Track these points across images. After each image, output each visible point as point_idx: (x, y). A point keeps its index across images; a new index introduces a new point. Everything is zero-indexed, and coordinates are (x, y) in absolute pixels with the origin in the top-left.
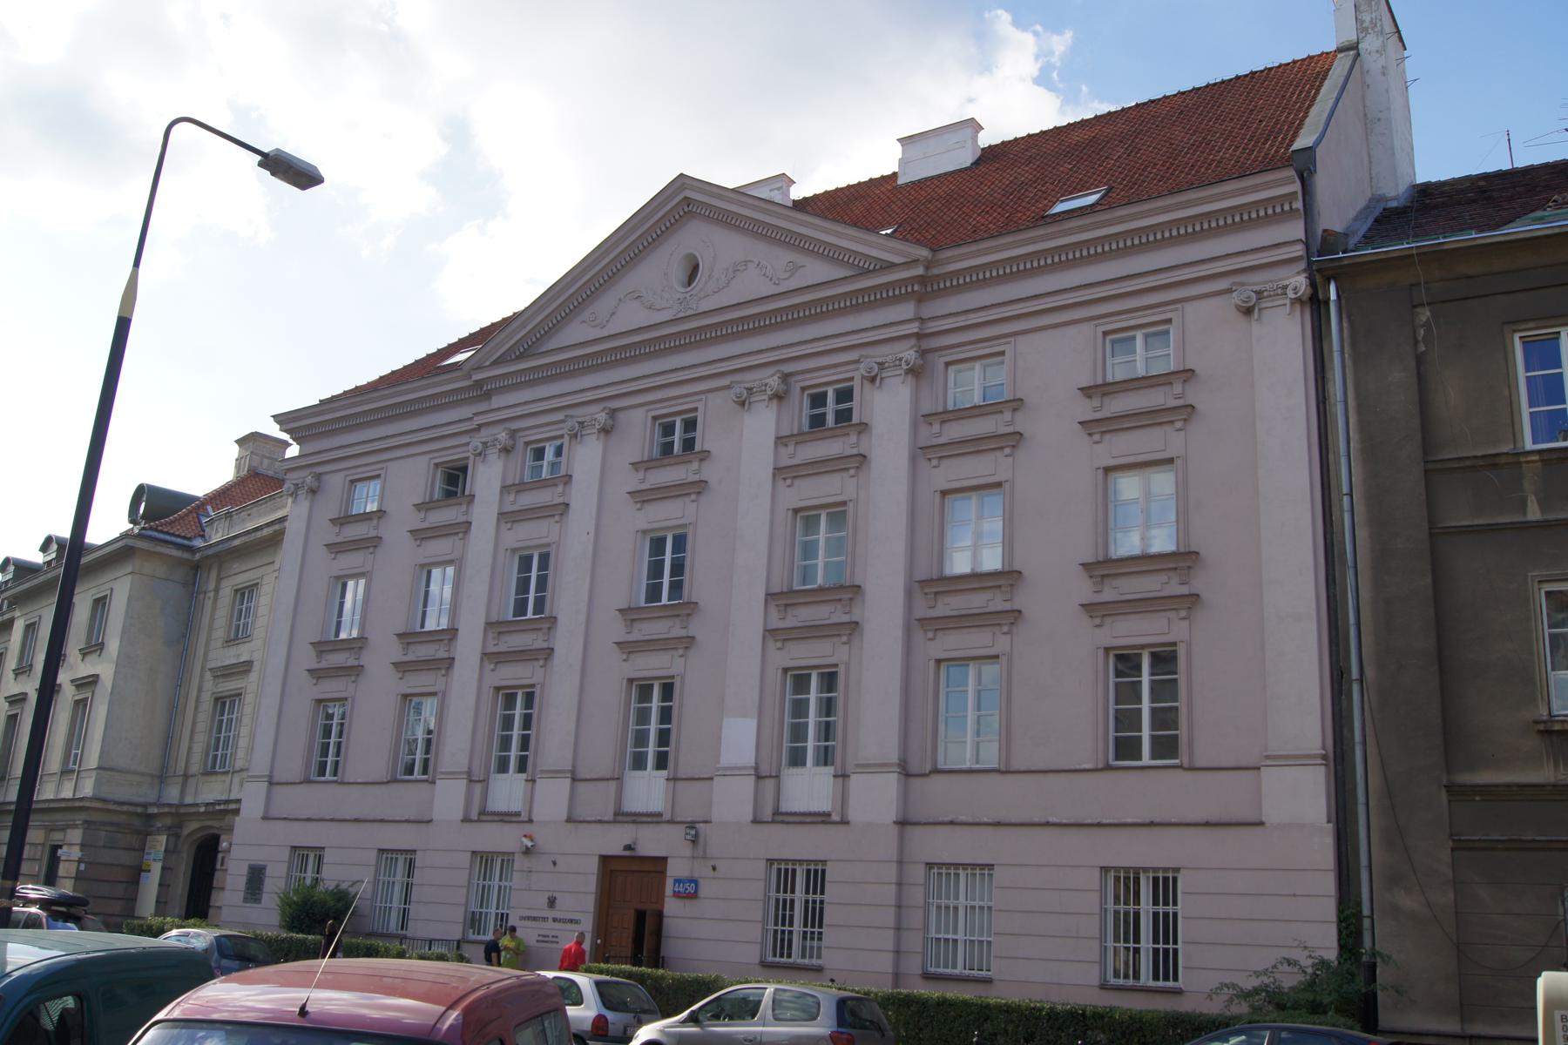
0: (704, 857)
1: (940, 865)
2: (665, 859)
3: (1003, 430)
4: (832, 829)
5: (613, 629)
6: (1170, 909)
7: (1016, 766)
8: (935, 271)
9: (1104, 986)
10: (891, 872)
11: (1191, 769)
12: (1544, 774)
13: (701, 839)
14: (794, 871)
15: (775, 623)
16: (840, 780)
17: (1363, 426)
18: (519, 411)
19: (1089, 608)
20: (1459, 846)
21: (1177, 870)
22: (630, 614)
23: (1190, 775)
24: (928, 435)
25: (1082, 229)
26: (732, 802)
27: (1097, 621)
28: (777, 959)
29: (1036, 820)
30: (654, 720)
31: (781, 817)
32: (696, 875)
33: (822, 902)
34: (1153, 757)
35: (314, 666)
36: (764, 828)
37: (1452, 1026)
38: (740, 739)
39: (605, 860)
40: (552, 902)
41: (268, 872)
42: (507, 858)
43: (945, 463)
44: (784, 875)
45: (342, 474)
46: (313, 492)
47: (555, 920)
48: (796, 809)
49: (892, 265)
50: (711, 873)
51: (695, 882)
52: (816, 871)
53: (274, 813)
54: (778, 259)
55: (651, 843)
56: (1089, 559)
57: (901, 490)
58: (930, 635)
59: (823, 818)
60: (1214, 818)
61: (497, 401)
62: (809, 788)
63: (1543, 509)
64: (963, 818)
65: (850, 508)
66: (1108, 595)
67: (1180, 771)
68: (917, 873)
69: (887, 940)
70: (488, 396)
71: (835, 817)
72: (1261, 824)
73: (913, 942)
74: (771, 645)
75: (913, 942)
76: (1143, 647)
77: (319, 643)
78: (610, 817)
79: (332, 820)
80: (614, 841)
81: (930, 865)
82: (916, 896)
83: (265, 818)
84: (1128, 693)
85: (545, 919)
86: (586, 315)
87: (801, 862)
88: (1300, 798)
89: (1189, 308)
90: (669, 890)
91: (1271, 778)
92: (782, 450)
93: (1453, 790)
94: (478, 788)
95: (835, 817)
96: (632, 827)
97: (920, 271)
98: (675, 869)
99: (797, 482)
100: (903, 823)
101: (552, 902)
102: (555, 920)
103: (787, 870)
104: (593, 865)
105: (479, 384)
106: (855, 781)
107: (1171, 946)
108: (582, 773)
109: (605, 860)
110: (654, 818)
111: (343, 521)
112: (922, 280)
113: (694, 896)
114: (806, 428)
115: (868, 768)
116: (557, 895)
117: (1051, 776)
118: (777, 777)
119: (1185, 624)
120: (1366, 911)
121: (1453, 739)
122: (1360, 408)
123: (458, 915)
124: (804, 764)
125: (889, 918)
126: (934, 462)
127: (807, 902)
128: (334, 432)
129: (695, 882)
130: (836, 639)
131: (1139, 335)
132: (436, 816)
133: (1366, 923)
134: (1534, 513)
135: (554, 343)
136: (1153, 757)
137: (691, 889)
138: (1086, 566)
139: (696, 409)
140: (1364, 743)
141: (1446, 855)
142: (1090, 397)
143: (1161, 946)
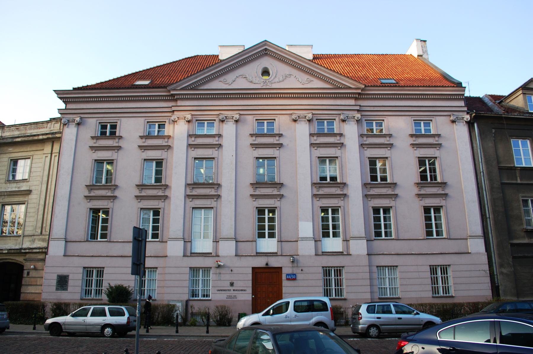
0: (297, 267)
1: (380, 266)
2: (281, 268)
3: (276, 142)
4: (345, 257)
5: (81, 191)
6: (101, 278)
7: (400, 238)
8: (363, 92)
9: (81, 299)
10: (367, 269)
11: (162, 242)
12: (526, 241)
13: (295, 261)
14: (93, 271)
15: (189, 193)
16: (280, 243)
17: (485, 156)
18: (372, 109)
19: (86, 197)
20: (514, 258)
21: (343, 267)
22: (90, 187)
23: (110, 244)
24: (192, 141)
25: (409, 90)
26: (306, 249)
27: (139, 201)
28: (337, 297)
29: (408, 253)
30: (266, 222)
31: (194, 255)
32: (295, 272)
33: (102, 280)
34: (101, 238)
35: (87, 194)
36: (186, 258)
37: (515, 299)
38: (306, 228)
39: (254, 269)
40: (232, 284)
41: (70, 277)
42: (207, 270)
43: (368, 149)
44: (327, 271)
45: (95, 119)
46: (78, 124)
47: (234, 290)
48: (199, 252)
49: (350, 88)
50: (301, 272)
51: (295, 275)
52: (101, 271)
53: (67, 254)
54: (304, 77)
55: (274, 262)
56: (88, 184)
57: (357, 155)
58: (191, 200)
59: (340, 254)
60: (457, 252)
61: (179, 103)
62: (333, 244)
63: (521, 180)
64: (385, 253)
65: (115, 162)
66: (92, 194)
67: (159, 243)
68: (375, 269)
69: (368, 289)
70: (176, 100)
71: (345, 253)
72: (167, 256)
73: (376, 289)
74: (315, 200)
75: (376, 289)
76: (432, 207)
77: (90, 185)
78: (255, 254)
79: (107, 256)
80: (260, 262)
81: (377, 267)
82: (375, 275)
83: (64, 256)
84: (261, 220)
85: (229, 290)
86: (222, 79)
87: (332, 267)
88: (478, 246)
89: (437, 118)
90: (284, 277)
91: (469, 241)
92: (190, 139)
93: (513, 245)
94: (189, 244)
95: (345, 253)
96: (266, 258)
97: (360, 91)
98: (286, 271)
99: (319, 148)
100: (368, 254)
101: (232, 284)
102: (234, 290)
103: (90, 271)
104: (250, 271)
105: (173, 95)
106: (351, 242)
107: (436, 286)
108: (69, 239)
109: (254, 269)
110: (274, 254)
111: (148, 136)
112: (359, 94)
113: (295, 279)
114: (99, 135)
115: (58, 239)
116: (234, 282)
117: (411, 241)
118: (191, 242)
119: (444, 201)
120: (495, 274)
121: (511, 234)
122: (483, 151)
123: (186, 290)
124: (265, 237)
125: (368, 282)
126: (366, 149)
127: (97, 280)
128: (276, 98)
129: (295, 275)
130: (339, 199)
131: (374, 122)
132: (168, 255)
133: (496, 276)
134: (519, 181)
135: (206, 87)
136: (101, 238)
137: (294, 277)
138: (137, 185)
139: (117, 122)
140: (491, 233)
141: (511, 259)
142: (142, 139)
143: (98, 288)
